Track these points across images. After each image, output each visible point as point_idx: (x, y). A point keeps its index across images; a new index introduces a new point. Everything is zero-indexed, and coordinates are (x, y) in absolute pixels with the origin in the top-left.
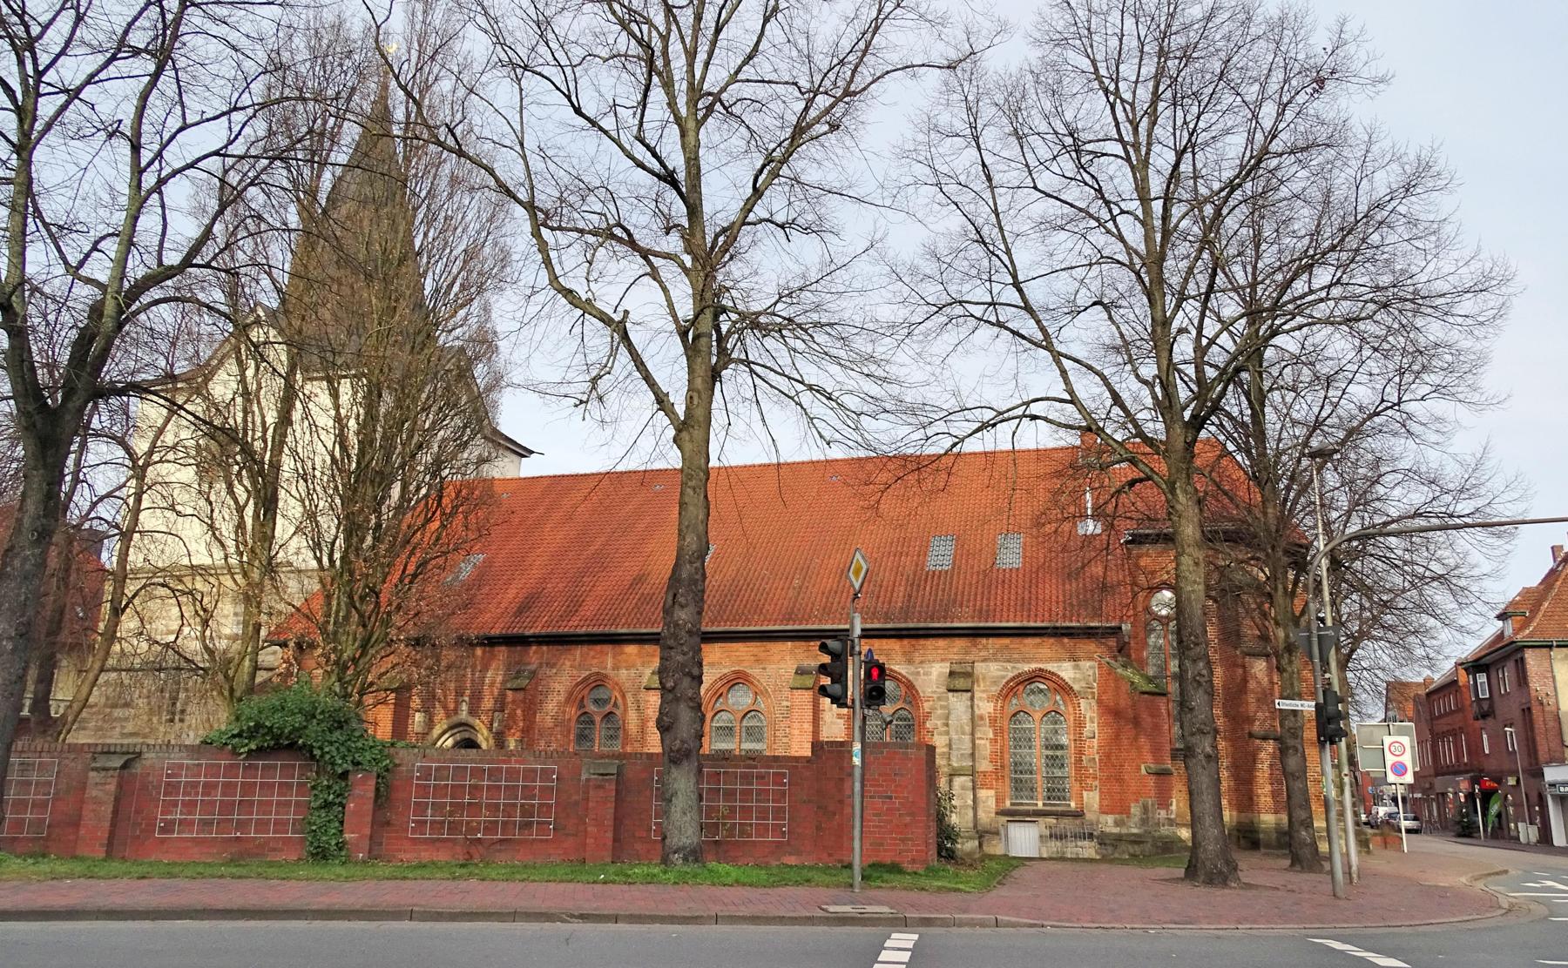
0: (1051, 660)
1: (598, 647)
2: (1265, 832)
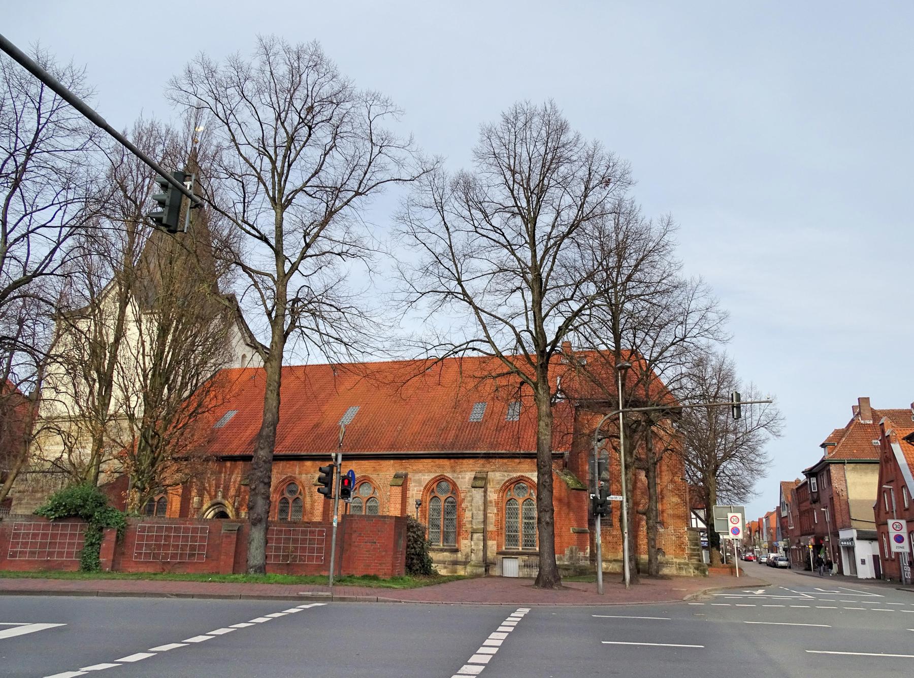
0: (528, 471)
1: (291, 462)
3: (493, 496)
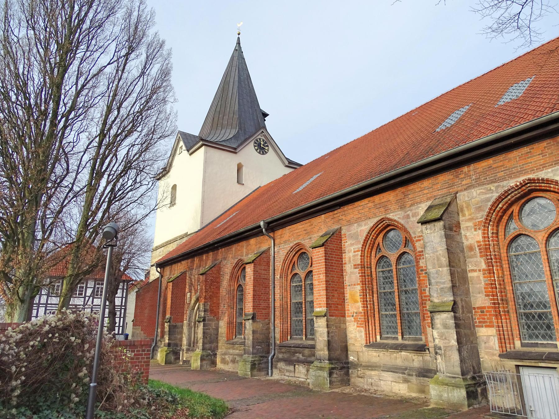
0: (544, 166)
3: (472, 235)
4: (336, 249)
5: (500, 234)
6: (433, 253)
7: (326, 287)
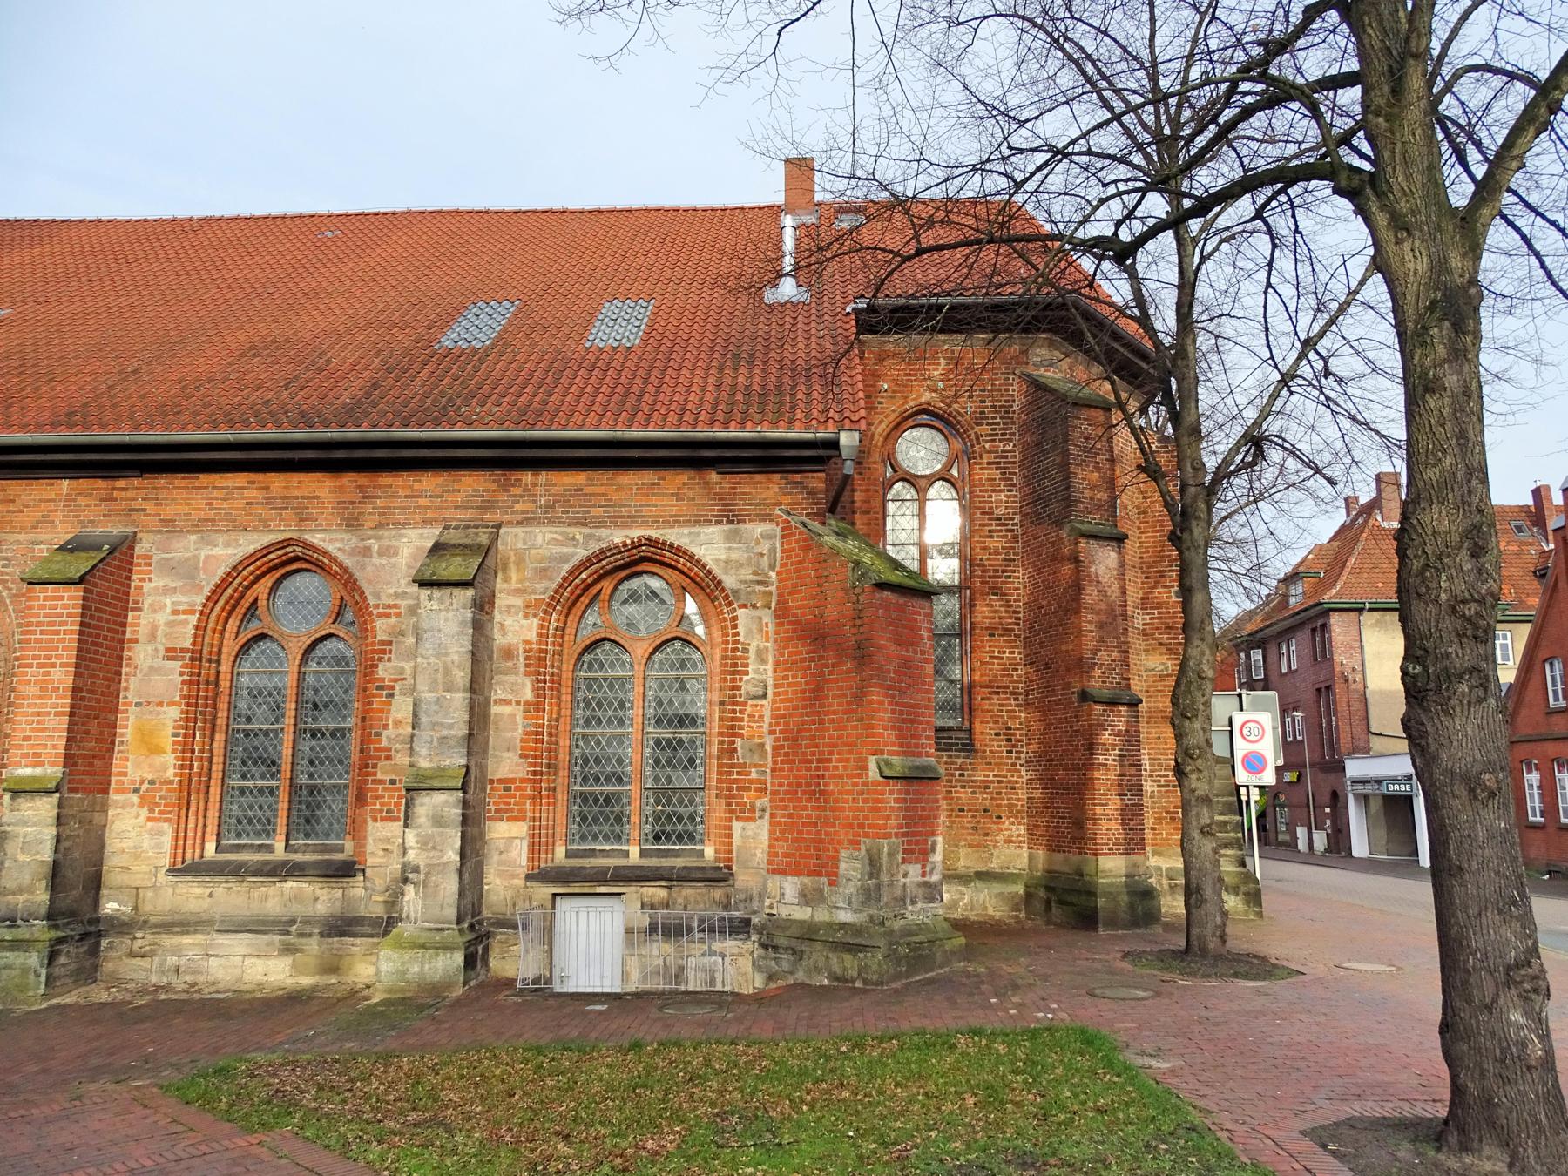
0: (676, 520)
2: (1111, 895)
3: (516, 627)
4: (113, 598)
5: (567, 631)
6: (437, 656)
7: (72, 706)
